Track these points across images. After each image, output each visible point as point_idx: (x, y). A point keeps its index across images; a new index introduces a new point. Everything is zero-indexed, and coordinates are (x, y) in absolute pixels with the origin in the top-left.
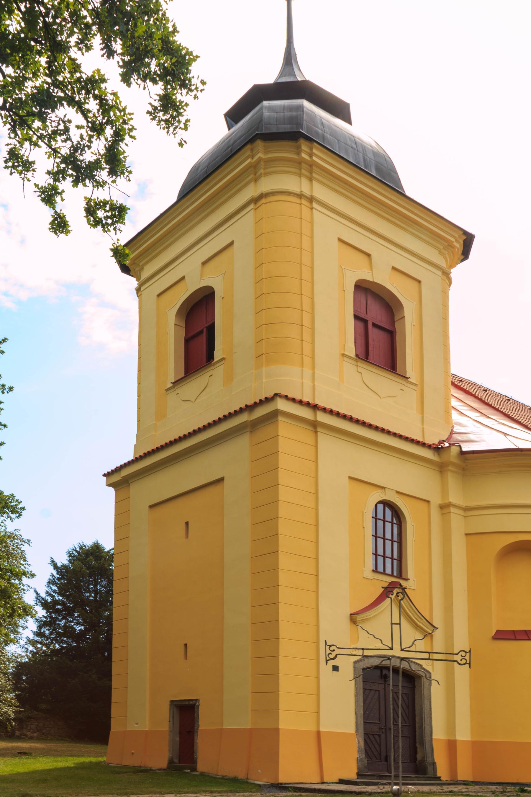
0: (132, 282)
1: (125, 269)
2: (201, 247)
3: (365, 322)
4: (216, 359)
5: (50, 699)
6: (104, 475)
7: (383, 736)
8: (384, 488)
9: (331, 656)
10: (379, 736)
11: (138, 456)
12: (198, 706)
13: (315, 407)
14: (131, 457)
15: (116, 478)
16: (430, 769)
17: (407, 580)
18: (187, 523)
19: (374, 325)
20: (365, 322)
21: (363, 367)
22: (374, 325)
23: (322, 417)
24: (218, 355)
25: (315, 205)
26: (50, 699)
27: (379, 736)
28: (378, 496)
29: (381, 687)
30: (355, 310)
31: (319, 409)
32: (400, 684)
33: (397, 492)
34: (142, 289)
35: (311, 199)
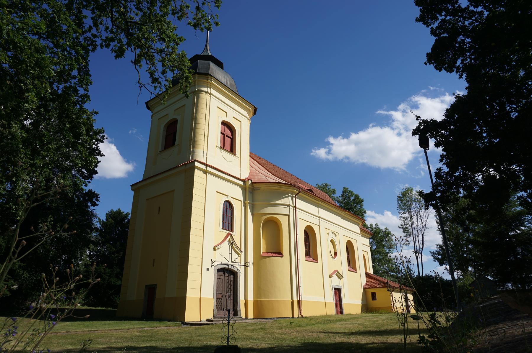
0: (150, 113)
1: (148, 108)
2: (173, 103)
3: (224, 134)
4: (176, 145)
5: (519, 249)
6: (131, 186)
7: (223, 299)
8: (227, 196)
9: (213, 265)
10: (222, 299)
11: (144, 179)
12: (156, 287)
13: (207, 165)
14: (142, 180)
15: (282, 256)
16: (239, 313)
17: (233, 232)
18: (159, 208)
19: (227, 136)
20: (224, 134)
21: (222, 151)
22: (227, 136)
23: (209, 169)
24: (176, 143)
25: (211, 95)
26: (519, 249)
27: (222, 299)
28: (225, 199)
29: (223, 278)
30: (221, 130)
31: (208, 166)
32: (85, 293)
33: (232, 197)
34: (154, 116)
35: (210, 94)
